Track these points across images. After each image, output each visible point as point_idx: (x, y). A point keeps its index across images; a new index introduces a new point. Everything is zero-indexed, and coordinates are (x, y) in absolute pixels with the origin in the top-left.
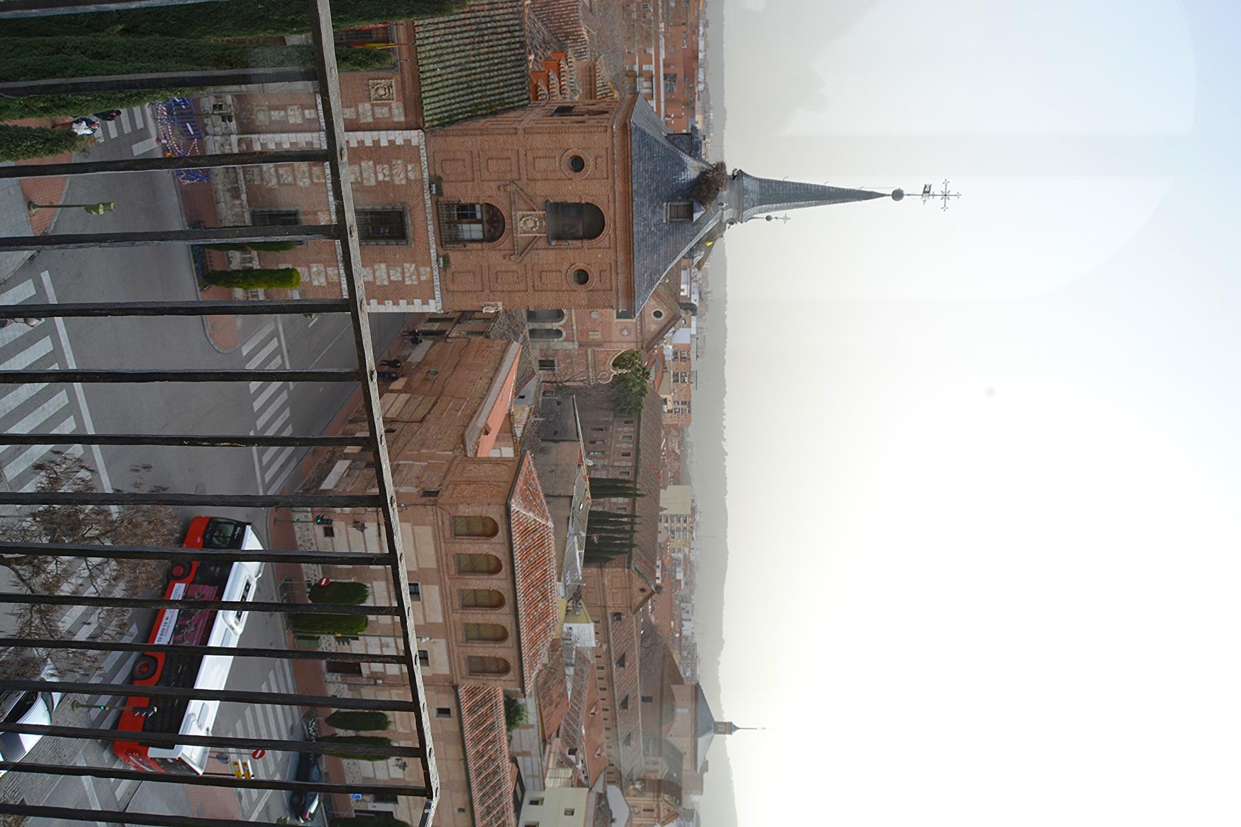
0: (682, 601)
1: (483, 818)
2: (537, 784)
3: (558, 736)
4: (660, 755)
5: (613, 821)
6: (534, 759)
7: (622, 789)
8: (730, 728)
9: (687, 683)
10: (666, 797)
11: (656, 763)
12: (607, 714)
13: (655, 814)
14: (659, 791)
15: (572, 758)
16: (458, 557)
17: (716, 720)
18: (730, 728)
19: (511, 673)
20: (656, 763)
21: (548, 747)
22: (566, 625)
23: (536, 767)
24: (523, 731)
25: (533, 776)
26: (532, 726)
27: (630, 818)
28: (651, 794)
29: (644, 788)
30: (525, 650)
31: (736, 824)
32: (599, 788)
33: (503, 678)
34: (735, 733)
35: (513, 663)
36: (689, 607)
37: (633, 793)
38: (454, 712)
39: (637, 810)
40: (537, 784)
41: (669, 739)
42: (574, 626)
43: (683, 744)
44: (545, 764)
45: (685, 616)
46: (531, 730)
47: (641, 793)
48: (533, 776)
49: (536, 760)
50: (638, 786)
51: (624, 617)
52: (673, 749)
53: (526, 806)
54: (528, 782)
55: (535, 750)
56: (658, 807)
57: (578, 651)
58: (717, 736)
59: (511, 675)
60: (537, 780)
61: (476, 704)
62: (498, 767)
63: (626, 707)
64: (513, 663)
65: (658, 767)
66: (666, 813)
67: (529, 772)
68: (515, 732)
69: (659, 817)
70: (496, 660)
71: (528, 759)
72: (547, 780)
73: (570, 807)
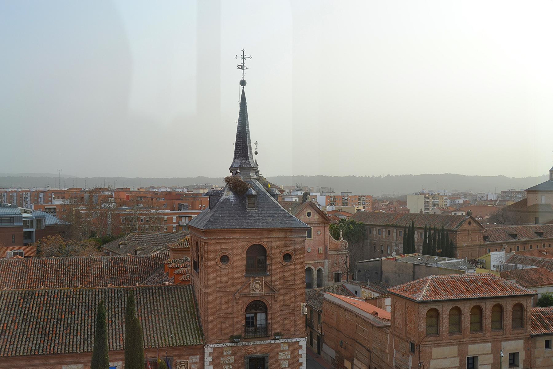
0: (476, 200)
12: (547, 244)
17: (548, 179)
19: (522, 302)
22: (492, 268)
30: (508, 294)
35: (516, 301)
36: (479, 196)
45: (485, 198)
57: (508, 261)
59: (524, 303)
64: (516, 301)
70: (514, 311)
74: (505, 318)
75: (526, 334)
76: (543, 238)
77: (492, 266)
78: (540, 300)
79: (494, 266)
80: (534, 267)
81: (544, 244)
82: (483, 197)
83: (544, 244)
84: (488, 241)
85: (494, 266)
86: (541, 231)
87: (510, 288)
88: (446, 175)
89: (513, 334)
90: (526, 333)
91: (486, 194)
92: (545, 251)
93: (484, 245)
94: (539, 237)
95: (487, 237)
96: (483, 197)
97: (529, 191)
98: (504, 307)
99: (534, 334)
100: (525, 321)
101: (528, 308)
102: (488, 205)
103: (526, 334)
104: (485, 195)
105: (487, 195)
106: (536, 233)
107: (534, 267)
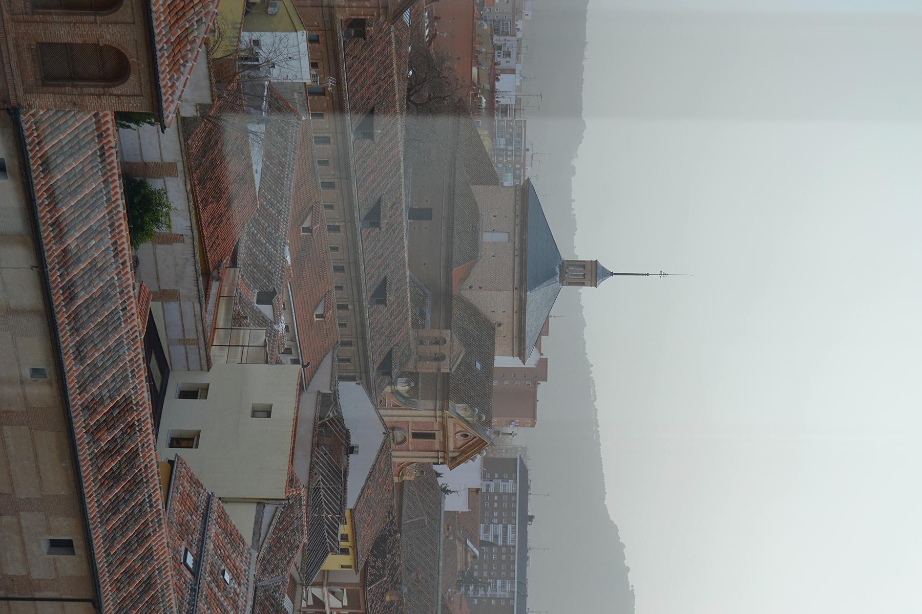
0: (496, 31)
1: (104, 523)
2: (193, 357)
3: (234, 263)
4: (448, 326)
5: (351, 450)
6: (187, 307)
7: (368, 389)
8: (592, 273)
9: (508, 181)
10: (460, 409)
11: (439, 342)
12: (337, 239)
13: (437, 444)
14: (446, 398)
15: (266, 310)
16: (44, 49)
17: (565, 256)
18: (592, 273)
19: (133, 78)
20: (439, 342)
21: (215, 285)
22: (246, 36)
23: (190, 323)
24: (161, 249)
25: (184, 342)
26: (179, 238)
27: (385, 449)
28: (430, 404)
29: (414, 392)
30: (160, 28)
31: (626, 598)
32: (321, 382)
33: (116, 90)
34: (606, 284)
35: (135, 57)
36: (510, 43)
37: (393, 401)
38: (78, 544)
39: (399, 435)
40: (193, 357)
41: (467, 294)
42: (266, 38)
43: (495, 303)
44: (209, 319)
45: (503, 62)
46: (178, 246)
47: (408, 401)
48: (184, 342)
49: (190, 307)
50: (402, 387)
51: (371, 30)
52: (473, 311)
53: (171, 402)
54: (175, 354)
55: (188, 285)
56: (444, 428)
57: (271, 88)
58: (566, 290)
59: (131, 84)
60: (192, 349)
61: (99, 427)
62: (150, 549)
63: (377, 224)
64: (135, 57)
65: (445, 350)
66: (460, 441)
67: (176, 333)
68: (145, 248)
69: (445, 449)
70: (100, 50)
71: (173, 306)
72: (214, 351)
73: (261, 400)
74: (73, 18)
75: (20, 92)
76: (358, 225)
77: (256, 36)
78: (143, 184)
79: (257, 43)
80: (257, 178)
81: (337, 229)
82: (508, 54)
83: (337, 229)
84: (347, 34)
85: (257, 43)
86: (384, 222)
87: (180, 40)
88: (616, 550)
89: (17, 46)
90: (26, 91)
91: (518, 68)
92: (314, 223)
93: (332, 18)
94: (364, 213)
95: (362, 34)
96: (508, 54)
97: (526, 195)
98: (112, 17)
99: (23, 118)
100: (68, 89)
101: (114, 99)
102: (478, 64)
103: (20, 92)
104: (512, 62)
105: (513, 71)
106: (379, 201)
107: (257, 178)
